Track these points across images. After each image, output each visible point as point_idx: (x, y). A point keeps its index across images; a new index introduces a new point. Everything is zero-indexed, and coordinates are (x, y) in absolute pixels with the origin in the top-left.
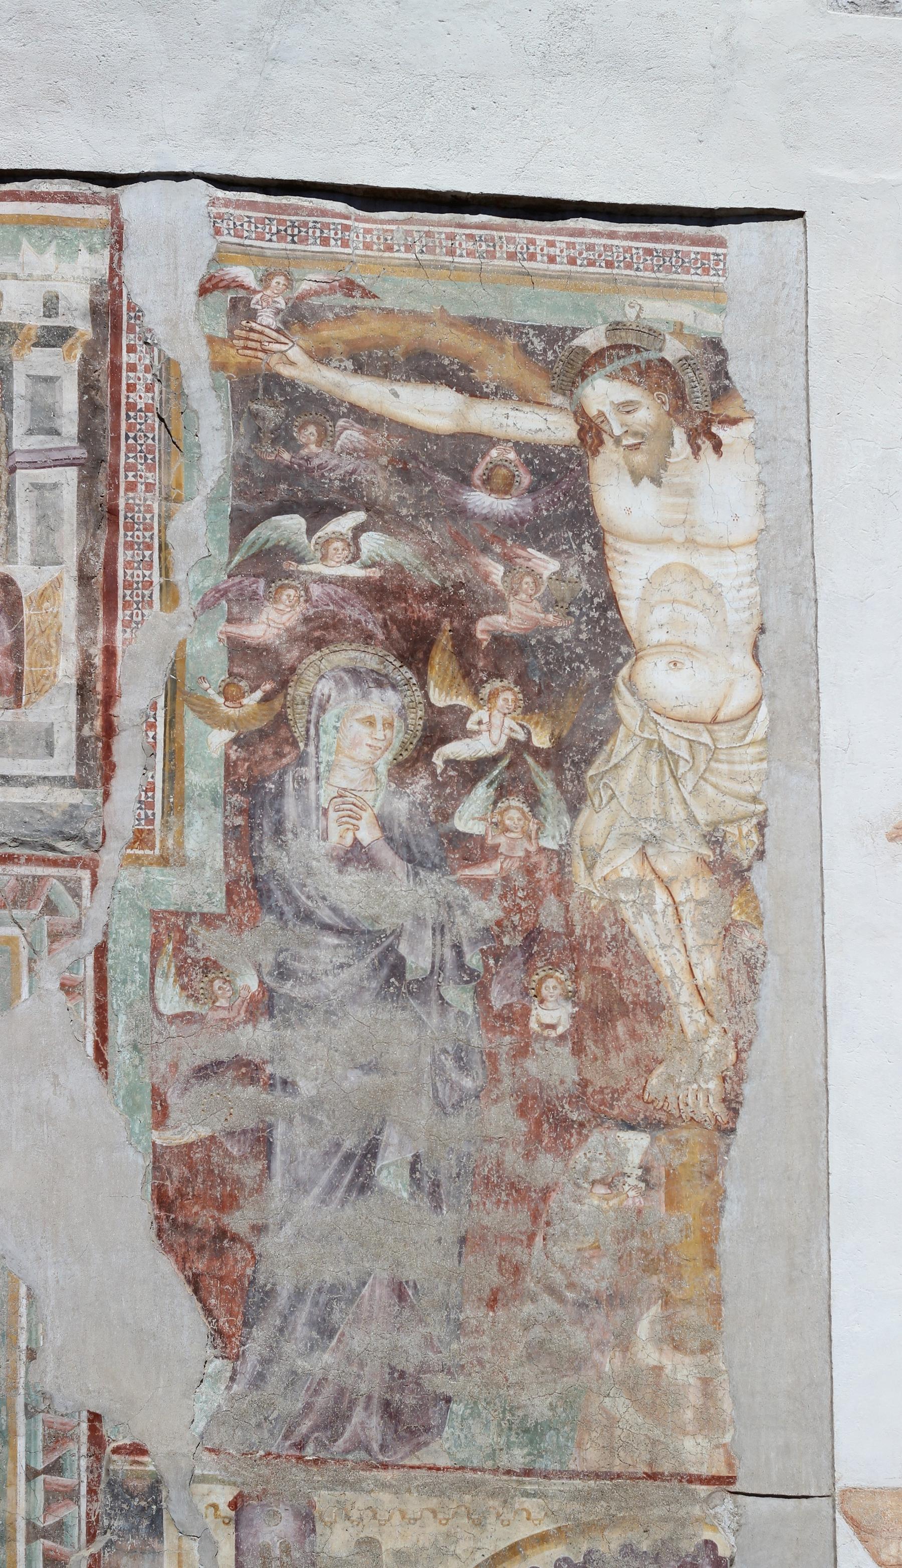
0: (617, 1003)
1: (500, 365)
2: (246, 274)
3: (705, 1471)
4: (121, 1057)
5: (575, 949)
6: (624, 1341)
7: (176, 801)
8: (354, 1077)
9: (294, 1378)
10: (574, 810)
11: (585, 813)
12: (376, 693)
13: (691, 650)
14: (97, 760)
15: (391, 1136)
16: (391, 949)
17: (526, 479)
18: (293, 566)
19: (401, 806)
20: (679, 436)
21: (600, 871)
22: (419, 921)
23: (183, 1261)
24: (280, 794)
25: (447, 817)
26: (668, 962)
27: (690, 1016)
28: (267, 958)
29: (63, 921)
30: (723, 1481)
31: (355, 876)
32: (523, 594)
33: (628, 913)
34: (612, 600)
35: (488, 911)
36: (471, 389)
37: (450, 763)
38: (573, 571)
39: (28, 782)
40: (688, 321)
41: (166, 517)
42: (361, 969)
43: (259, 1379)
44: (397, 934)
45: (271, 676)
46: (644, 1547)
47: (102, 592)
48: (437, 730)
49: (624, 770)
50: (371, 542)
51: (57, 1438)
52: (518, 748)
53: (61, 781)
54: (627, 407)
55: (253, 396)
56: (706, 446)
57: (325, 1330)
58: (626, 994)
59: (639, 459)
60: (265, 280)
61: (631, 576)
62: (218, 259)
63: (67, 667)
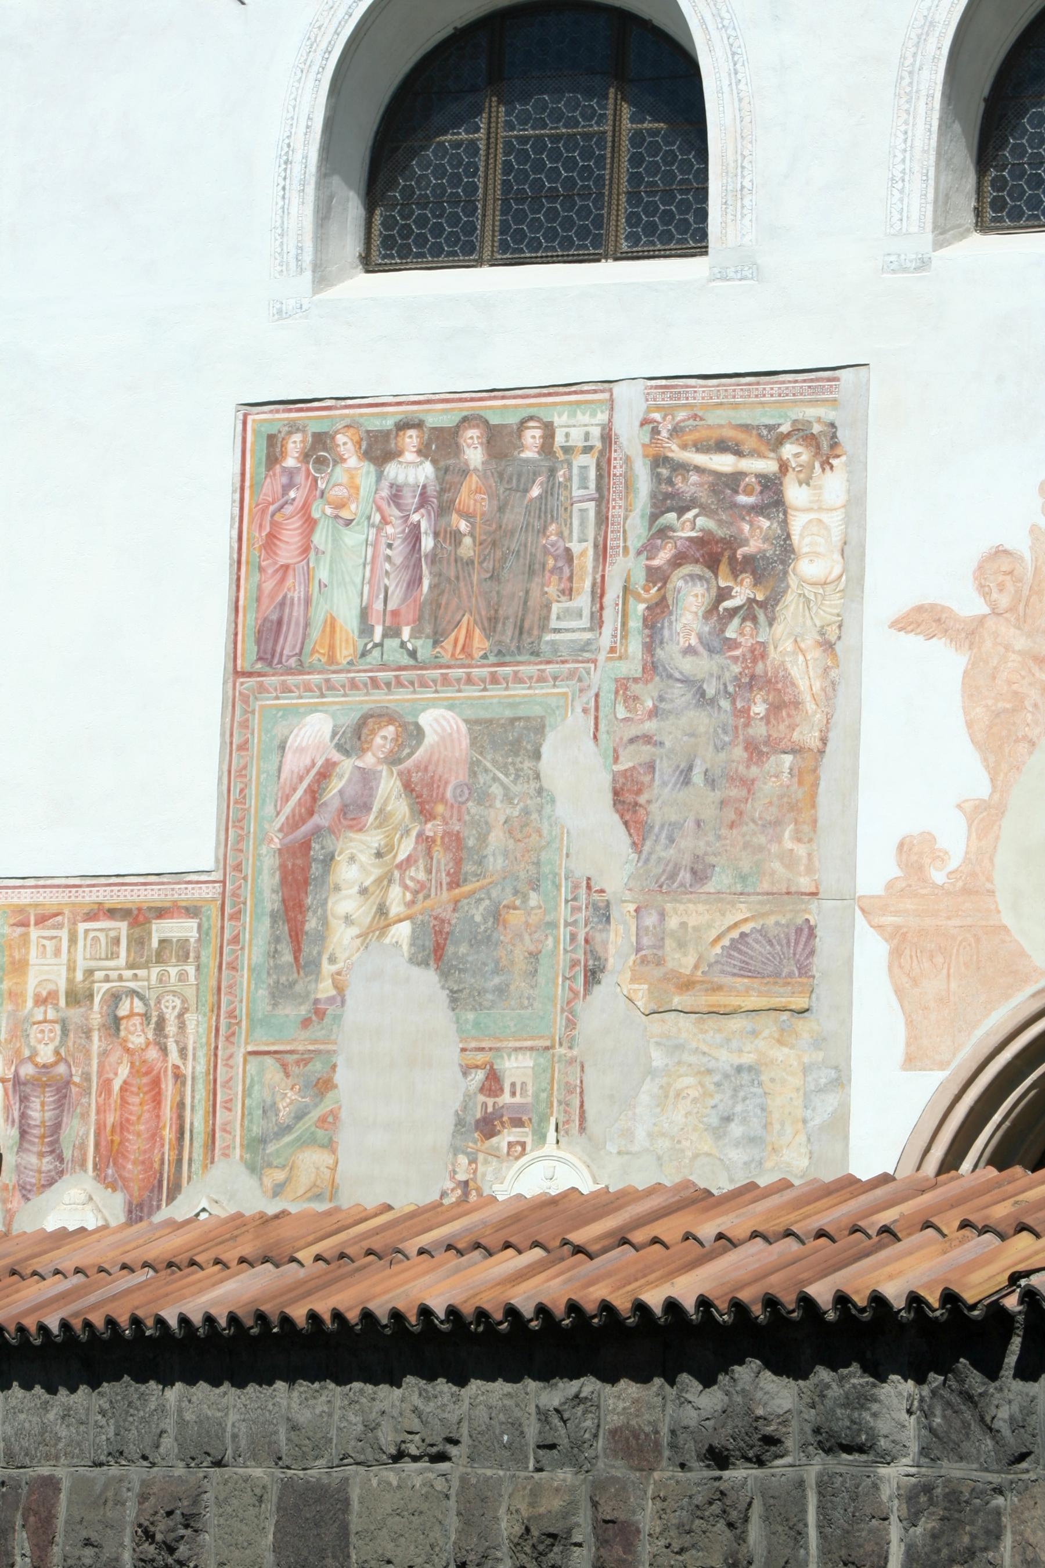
0: (785, 704)
1: (750, 442)
2: (657, 416)
3: (807, 891)
4: (602, 736)
5: (769, 682)
6: (779, 840)
7: (625, 636)
8: (685, 738)
9: (659, 860)
10: (771, 625)
11: (775, 625)
12: (699, 583)
13: (818, 554)
14: (597, 621)
15: (698, 762)
16: (701, 687)
17: (758, 488)
18: (671, 534)
19: (707, 629)
20: (817, 465)
21: (780, 649)
22: (711, 675)
23: (622, 816)
24: (662, 628)
25: (723, 631)
26: (802, 684)
27: (810, 706)
28: (655, 694)
29: (585, 684)
30: (814, 894)
31: (689, 659)
32: (755, 537)
33: (789, 666)
34: (789, 537)
35: (736, 669)
36: (739, 453)
37: (725, 610)
38: (775, 525)
39: (573, 630)
40: (823, 415)
41: (626, 518)
42: (689, 696)
43: (647, 860)
44: (703, 681)
45: (661, 580)
46: (783, 922)
47: (602, 552)
48: (723, 594)
49: (790, 606)
50: (701, 521)
51: (576, 887)
52: (751, 601)
53: (584, 630)
54: (797, 455)
55: (658, 466)
56: (827, 468)
57: (671, 840)
58: (786, 699)
59: (802, 476)
60: (664, 418)
61: (797, 524)
62: (649, 410)
63: (588, 584)
